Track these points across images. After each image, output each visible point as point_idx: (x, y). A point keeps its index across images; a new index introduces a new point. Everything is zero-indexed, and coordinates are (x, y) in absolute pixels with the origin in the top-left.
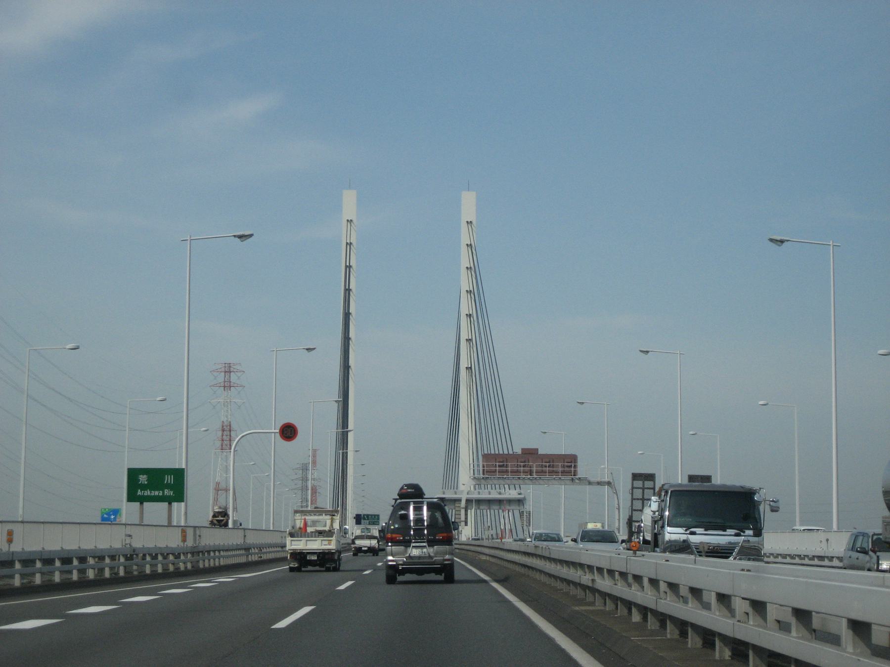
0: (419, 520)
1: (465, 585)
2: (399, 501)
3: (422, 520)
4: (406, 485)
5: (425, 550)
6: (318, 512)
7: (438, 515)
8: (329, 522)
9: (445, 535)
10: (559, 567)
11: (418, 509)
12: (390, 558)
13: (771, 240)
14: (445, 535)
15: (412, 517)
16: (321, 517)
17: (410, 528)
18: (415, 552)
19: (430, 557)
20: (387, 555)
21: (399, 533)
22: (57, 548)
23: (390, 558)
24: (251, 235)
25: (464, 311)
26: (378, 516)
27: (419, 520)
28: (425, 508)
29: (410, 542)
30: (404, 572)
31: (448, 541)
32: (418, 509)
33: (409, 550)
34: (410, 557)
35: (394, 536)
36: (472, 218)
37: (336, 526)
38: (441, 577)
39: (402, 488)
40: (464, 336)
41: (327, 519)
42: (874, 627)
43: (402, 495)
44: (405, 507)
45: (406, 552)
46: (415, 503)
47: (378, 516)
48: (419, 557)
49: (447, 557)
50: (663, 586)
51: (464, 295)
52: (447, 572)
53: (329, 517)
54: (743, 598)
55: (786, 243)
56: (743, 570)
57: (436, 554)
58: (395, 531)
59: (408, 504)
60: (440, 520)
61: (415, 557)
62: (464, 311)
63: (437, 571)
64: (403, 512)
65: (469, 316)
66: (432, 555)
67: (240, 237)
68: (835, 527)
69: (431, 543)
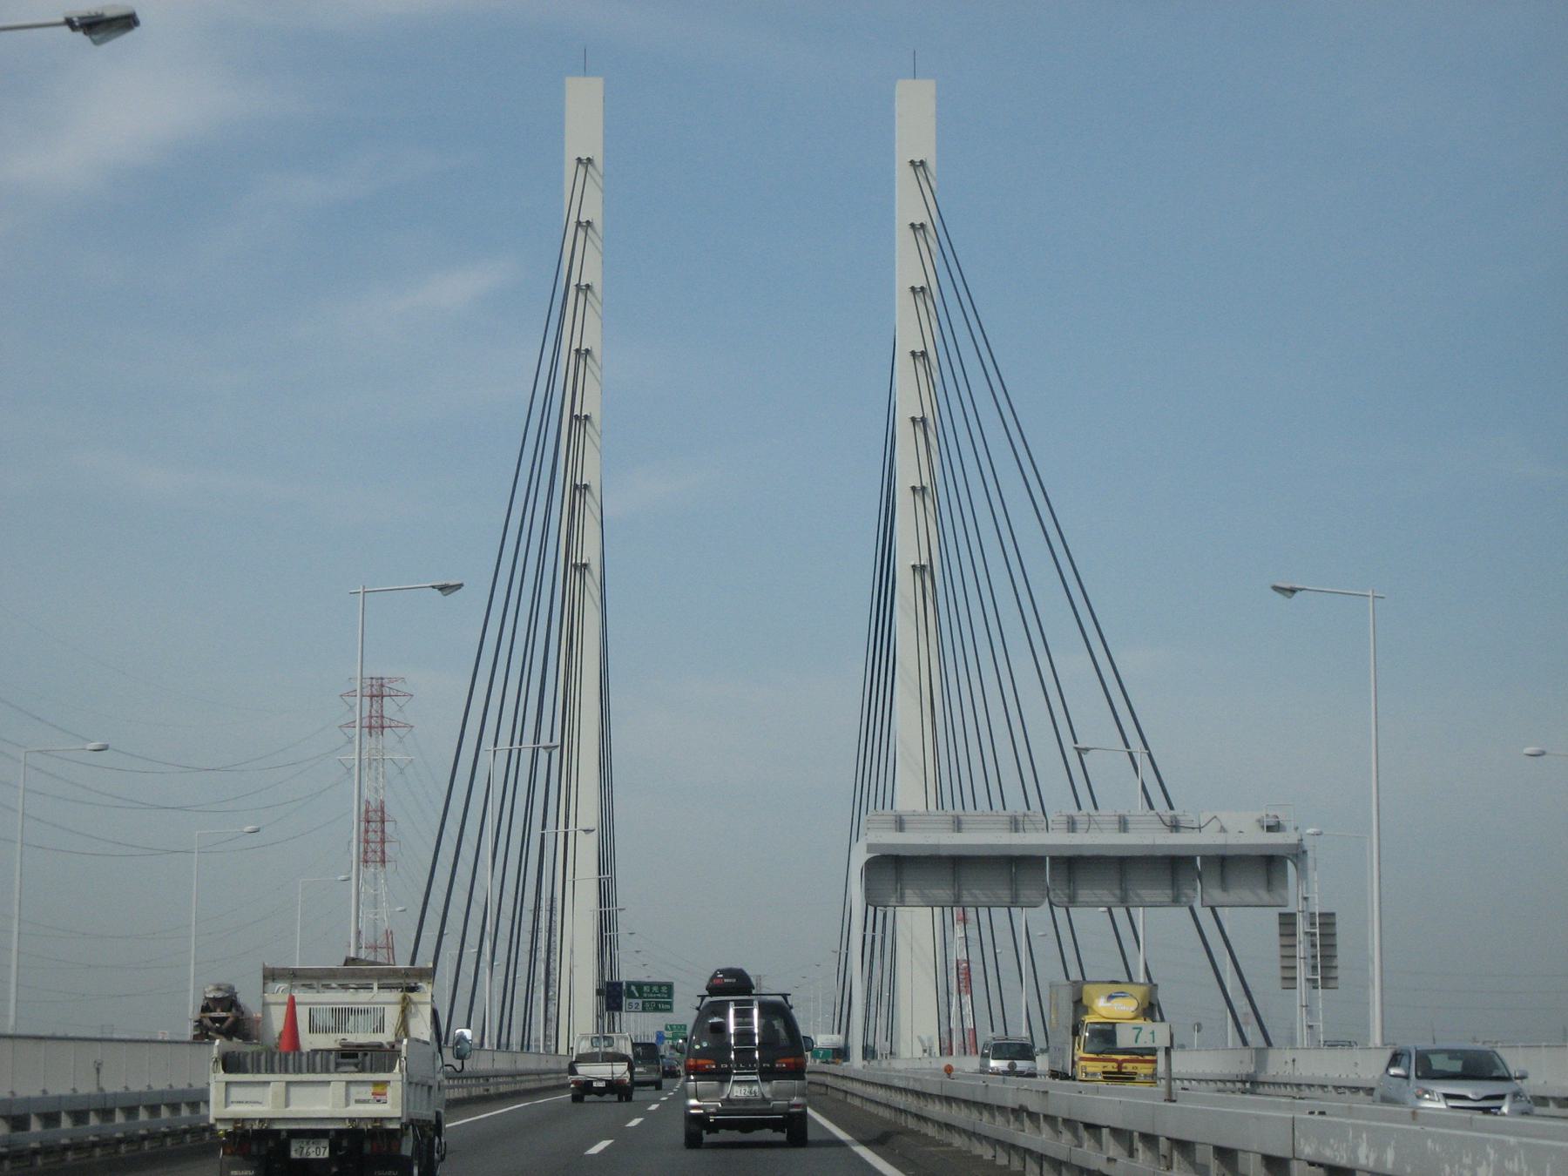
0: (744, 1035)
1: (822, 1150)
2: (708, 999)
3: (751, 1034)
4: (722, 971)
5: (755, 1088)
6: (353, 975)
7: (778, 1024)
8: (392, 1015)
9: (791, 1060)
10: (975, 1115)
11: (744, 1014)
12: (693, 1102)
13: (1276, 588)
14: (791, 1060)
15: (732, 1028)
16: (363, 996)
17: (728, 1047)
18: (738, 1092)
19: (764, 1100)
20: (688, 1097)
21: (713, 1059)
22: (35, 1093)
23: (693, 1102)
24: (460, 586)
25: (908, 407)
26: (670, 986)
27: (744, 1035)
28: (756, 1012)
29: (728, 1073)
30: (714, 1127)
31: (797, 1072)
32: (744, 1014)
33: (728, 1088)
34: (728, 1100)
35: (700, 1062)
36: (928, 154)
37: (421, 1028)
38: (781, 1136)
39: (714, 976)
40: (907, 477)
41: (388, 1001)
42: (1240, 1155)
43: (713, 989)
44: (721, 1010)
45: (721, 1091)
46: (737, 1003)
47: (670, 986)
48: (746, 1101)
49: (796, 1100)
50: (1163, 1145)
51: (904, 362)
52: (794, 1129)
53: (396, 996)
54: (1312, 1164)
55: (1298, 594)
56: (1312, 1113)
57: (776, 1094)
58: (702, 1054)
59: (725, 1004)
60: (783, 1033)
61: (739, 1101)
62: (908, 407)
63: (776, 1126)
64: (716, 1020)
65: (920, 422)
66: (768, 1096)
67: (442, 588)
68: (263, 1058)
69: (767, 1075)
